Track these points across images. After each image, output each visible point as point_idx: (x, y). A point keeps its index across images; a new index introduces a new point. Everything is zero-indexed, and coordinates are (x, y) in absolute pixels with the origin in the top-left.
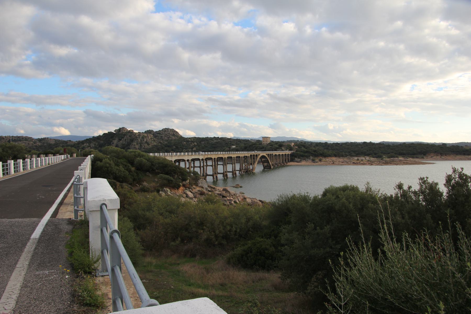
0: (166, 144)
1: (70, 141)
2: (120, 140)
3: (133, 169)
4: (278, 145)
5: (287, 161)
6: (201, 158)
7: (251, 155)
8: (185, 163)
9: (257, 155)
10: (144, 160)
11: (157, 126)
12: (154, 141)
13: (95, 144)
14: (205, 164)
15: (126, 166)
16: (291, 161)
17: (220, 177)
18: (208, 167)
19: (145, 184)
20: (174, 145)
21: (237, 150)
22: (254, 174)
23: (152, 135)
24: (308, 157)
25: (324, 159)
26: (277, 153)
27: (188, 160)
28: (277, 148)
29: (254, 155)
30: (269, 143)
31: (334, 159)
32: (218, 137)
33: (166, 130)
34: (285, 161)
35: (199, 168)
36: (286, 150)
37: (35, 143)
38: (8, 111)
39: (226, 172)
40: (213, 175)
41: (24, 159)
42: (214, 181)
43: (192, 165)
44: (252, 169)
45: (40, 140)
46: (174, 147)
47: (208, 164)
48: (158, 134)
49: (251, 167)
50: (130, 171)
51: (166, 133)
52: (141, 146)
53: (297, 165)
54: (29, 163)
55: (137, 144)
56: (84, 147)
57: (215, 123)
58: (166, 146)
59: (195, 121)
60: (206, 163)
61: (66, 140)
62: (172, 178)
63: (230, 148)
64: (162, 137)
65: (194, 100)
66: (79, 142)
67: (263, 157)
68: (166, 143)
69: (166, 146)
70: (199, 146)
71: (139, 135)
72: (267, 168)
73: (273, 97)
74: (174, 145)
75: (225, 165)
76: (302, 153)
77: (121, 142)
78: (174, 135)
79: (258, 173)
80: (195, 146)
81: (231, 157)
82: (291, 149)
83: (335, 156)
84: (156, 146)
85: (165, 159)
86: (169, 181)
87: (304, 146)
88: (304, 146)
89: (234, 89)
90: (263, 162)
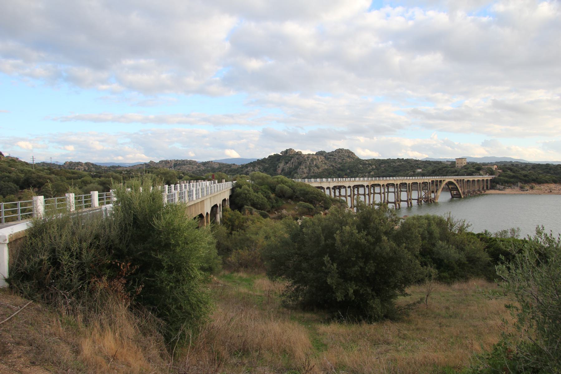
0: (340, 167)
1: (234, 164)
2: (287, 163)
3: (272, 196)
4: (475, 168)
5: (485, 188)
6: (365, 184)
7: (433, 181)
8: (346, 190)
9: (441, 181)
10: (286, 187)
11: (331, 147)
12: (325, 164)
13: (260, 168)
14: (356, 192)
15: (265, 192)
16: (491, 189)
17: (404, 205)
18: (376, 195)
19: (284, 212)
20: (349, 168)
21: (423, 175)
22: (436, 204)
23: (323, 157)
24: (514, 184)
25: (537, 187)
26: (471, 178)
27: (349, 187)
28: (473, 172)
30: (465, 166)
31: (553, 186)
32: (403, 159)
33: (339, 151)
34: (483, 188)
35: (363, 197)
36: (486, 174)
37: (199, 167)
38: (184, 133)
39: (410, 199)
40: (407, 201)
41: (175, 184)
43: (372, 191)
44: (435, 198)
45: (204, 164)
46: (348, 171)
47: (376, 191)
48: (330, 155)
49: (433, 196)
50: (269, 198)
51: (340, 154)
52: (310, 170)
53: (498, 194)
54: (179, 187)
55: (306, 168)
56: (248, 171)
57: (408, 142)
58: (338, 170)
59: (384, 138)
60: (388, 189)
61: (230, 163)
62: (312, 206)
63: (414, 172)
64: (335, 159)
65: (388, 111)
66: (242, 165)
67: (450, 183)
68: (339, 166)
69: (339, 169)
70: (378, 170)
71: (308, 157)
73: (497, 105)
74: (349, 168)
75: (420, 190)
76: (506, 179)
77: (288, 165)
78: (349, 157)
79: (444, 203)
80: (373, 169)
82: (491, 173)
83: (555, 182)
84: (327, 169)
85: (309, 186)
86: (309, 209)
87: (511, 170)
88: (511, 170)
89: (446, 97)
90: (451, 190)
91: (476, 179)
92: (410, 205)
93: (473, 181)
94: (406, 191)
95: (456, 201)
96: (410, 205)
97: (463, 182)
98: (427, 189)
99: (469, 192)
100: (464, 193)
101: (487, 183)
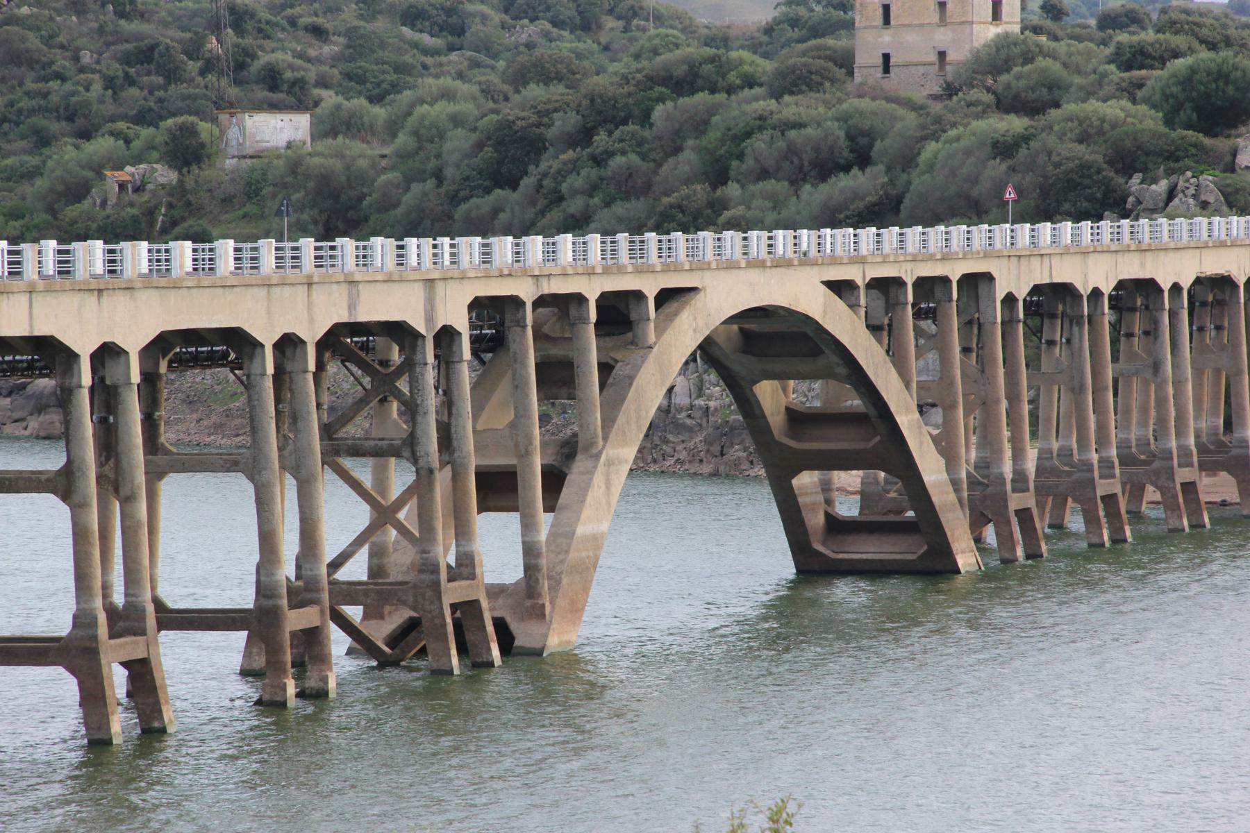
7: (493, 313)
9: (618, 314)
21: (337, 210)
22: (556, 683)
26: (1088, 257)
28: (1131, 157)
29: (563, 306)
39: (125, 621)
40: (74, 653)
42: (98, 743)
44: (530, 593)
49: (498, 547)
63: (187, 153)
67: (770, 338)
72: (877, 555)
81: (233, 345)
90: (781, 458)
91: (1175, 271)
92: (121, 724)
93: (1137, 295)
94: (63, 484)
95: (840, 631)
96: (121, 724)
97: (973, 325)
98: (409, 448)
99: (1062, 483)
100: (985, 504)
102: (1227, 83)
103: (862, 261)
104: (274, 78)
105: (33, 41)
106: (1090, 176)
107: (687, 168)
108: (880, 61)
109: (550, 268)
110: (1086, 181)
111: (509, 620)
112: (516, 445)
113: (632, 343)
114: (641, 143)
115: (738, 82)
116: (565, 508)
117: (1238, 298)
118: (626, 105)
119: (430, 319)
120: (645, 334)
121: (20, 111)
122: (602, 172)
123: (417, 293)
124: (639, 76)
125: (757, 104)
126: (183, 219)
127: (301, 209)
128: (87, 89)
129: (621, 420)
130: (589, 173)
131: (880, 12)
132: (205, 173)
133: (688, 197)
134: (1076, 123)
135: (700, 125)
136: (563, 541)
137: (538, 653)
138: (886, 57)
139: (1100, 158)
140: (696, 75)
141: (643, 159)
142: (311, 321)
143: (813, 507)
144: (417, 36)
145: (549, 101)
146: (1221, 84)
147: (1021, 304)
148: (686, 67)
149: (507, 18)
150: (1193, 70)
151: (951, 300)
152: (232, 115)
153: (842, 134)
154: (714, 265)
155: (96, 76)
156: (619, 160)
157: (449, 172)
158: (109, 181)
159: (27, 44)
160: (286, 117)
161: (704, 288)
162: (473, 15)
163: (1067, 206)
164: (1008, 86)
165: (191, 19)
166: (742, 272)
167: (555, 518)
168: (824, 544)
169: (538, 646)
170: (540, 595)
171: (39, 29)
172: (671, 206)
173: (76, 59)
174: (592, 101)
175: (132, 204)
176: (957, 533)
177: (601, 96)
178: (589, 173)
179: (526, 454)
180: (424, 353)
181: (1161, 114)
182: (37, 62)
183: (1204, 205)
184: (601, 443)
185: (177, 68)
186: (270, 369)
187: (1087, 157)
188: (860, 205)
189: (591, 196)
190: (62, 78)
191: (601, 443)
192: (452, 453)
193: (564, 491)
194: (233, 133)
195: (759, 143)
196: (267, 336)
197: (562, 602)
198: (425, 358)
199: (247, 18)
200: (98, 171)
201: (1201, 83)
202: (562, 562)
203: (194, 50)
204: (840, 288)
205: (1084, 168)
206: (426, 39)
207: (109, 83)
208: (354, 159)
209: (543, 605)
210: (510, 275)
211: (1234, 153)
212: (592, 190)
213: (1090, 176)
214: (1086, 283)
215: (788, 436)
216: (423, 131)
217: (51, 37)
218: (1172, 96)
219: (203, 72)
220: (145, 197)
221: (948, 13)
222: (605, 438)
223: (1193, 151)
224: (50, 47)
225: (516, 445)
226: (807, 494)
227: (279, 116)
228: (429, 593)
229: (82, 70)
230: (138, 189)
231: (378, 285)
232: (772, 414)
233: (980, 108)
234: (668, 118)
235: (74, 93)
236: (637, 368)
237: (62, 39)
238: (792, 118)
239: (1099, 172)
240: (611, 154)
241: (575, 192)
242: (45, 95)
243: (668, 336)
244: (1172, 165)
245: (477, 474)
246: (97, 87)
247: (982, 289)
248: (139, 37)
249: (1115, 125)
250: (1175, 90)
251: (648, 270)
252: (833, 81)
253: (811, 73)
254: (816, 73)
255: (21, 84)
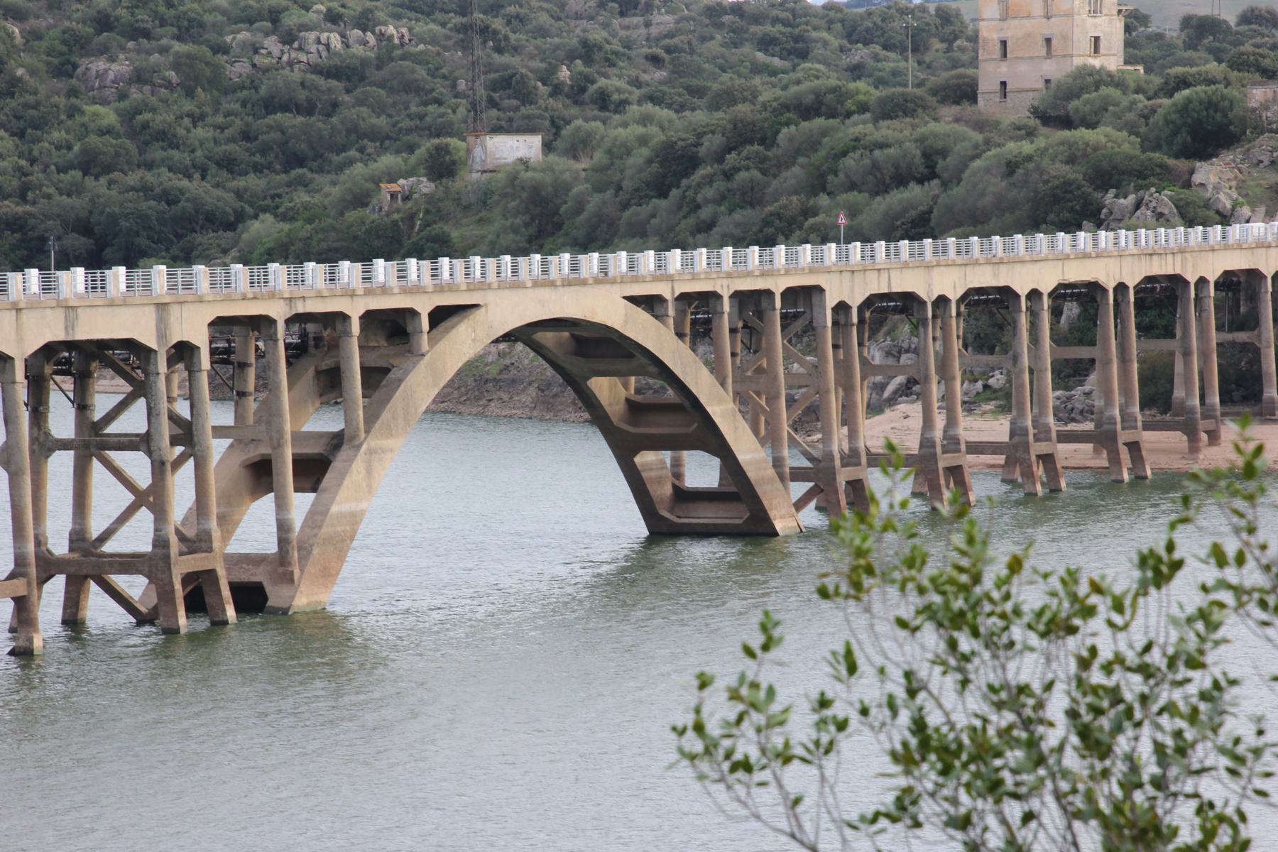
5: (1197, 377)
9: (392, 327)
22: (322, 647)
26: (1114, 257)
28: (1109, 175)
44: (281, 564)
63: (442, 167)
101: (1034, 315)
102: (1216, 111)
103: (670, 279)
104: (604, 100)
105: (421, 73)
106: (1071, 192)
107: (793, 181)
108: (998, 87)
109: (301, 291)
110: (1068, 196)
111: (265, 584)
112: (271, 439)
113: (409, 351)
114: (763, 160)
115: (854, 108)
116: (325, 490)
117: (1107, 299)
118: (762, 128)
119: (161, 335)
120: (419, 345)
121: (400, 130)
122: (730, 185)
123: (149, 315)
124: (775, 104)
125: (860, 127)
126: (435, 222)
127: (515, 216)
128: (454, 112)
129: (386, 415)
130: (720, 185)
131: (998, 46)
132: (457, 185)
133: (785, 207)
134: (1066, 147)
135: (813, 144)
136: (318, 518)
137: (285, 612)
138: (1004, 84)
139: (1080, 177)
140: (821, 103)
141: (764, 174)
142: (20, 340)
143: (659, 480)
144: (769, 59)
145: (707, 125)
146: (1211, 112)
147: (1132, 292)
148: (812, 96)
149: (845, 42)
150: (1189, 100)
151: (774, 309)
152: (477, 137)
153: (918, 152)
154: (495, 285)
155: (464, 101)
156: (743, 175)
157: (627, 184)
158: (383, 192)
159: (416, 75)
160: (522, 138)
161: (486, 305)
162: (816, 41)
163: (1052, 217)
164: (1077, 110)
165: (554, 51)
166: (530, 291)
167: (316, 498)
168: (671, 511)
169: (285, 605)
170: (290, 564)
171: (428, 63)
172: (772, 214)
173: (454, 86)
174: (735, 125)
175: (398, 211)
176: (775, 502)
177: (742, 121)
178: (720, 185)
179: (278, 446)
180: (156, 365)
181: (1139, 140)
182: (423, 89)
183: (1159, 216)
184: (363, 435)
185: (530, 93)
186: (1193, 295)
187: (1069, 176)
188: (913, 213)
189: (720, 205)
190: (439, 102)
191: (363, 435)
192: (193, 447)
193: (328, 475)
194: (477, 152)
195: (849, 162)
196: (1192, 279)
197: (310, 569)
198: (156, 367)
199: (595, 49)
200: (377, 182)
201: (1194, 110)
202: (315, 535)
203: (546, 77)
204: (650, 303)
205: (1067, 185)
206: (777, 62)
207: (474, 106)
208: (562, 172)
209: (292, 572)
210: (255, 298)
211: (1192, 172)
212: (721, 198)
213: (1071, 192)
214: (930, 291)
215: (629, 423)
216: (615, 150)
217: (437, 69)
218: (1173, 122)
219: (552, 95)
220: (410, 204)
221: (1053, 48)
222: (367, 431)
223: (1158, 170)
224: (433, 76)
225: (271, 439)
226: (651, 469)
227: (515, 138)
228: (161, 564)
229: (456, 96)
230: (406, 198)
231: (100, 310)
232: (610, 405)
233: (1023, 132)
234: (791, 140)
235: (442, 115)
236: (407, 373)
237: (443, 71)
238: (880, 140)
239: (1079, 188)
240: (737, 170)
241: (707, 201)
242: (421, 118)
243: (443, 345)
244: (1140, 182)
245: (294, 461)
246: (462, 111)
247: (815, 300)
248: (506, 67)
249: (1096, 149)
250: (1174, 117)
251: (418, 290)
252: (924, 108)
253: (906, 101)
254: (912, 101)
255: (407, 108)
